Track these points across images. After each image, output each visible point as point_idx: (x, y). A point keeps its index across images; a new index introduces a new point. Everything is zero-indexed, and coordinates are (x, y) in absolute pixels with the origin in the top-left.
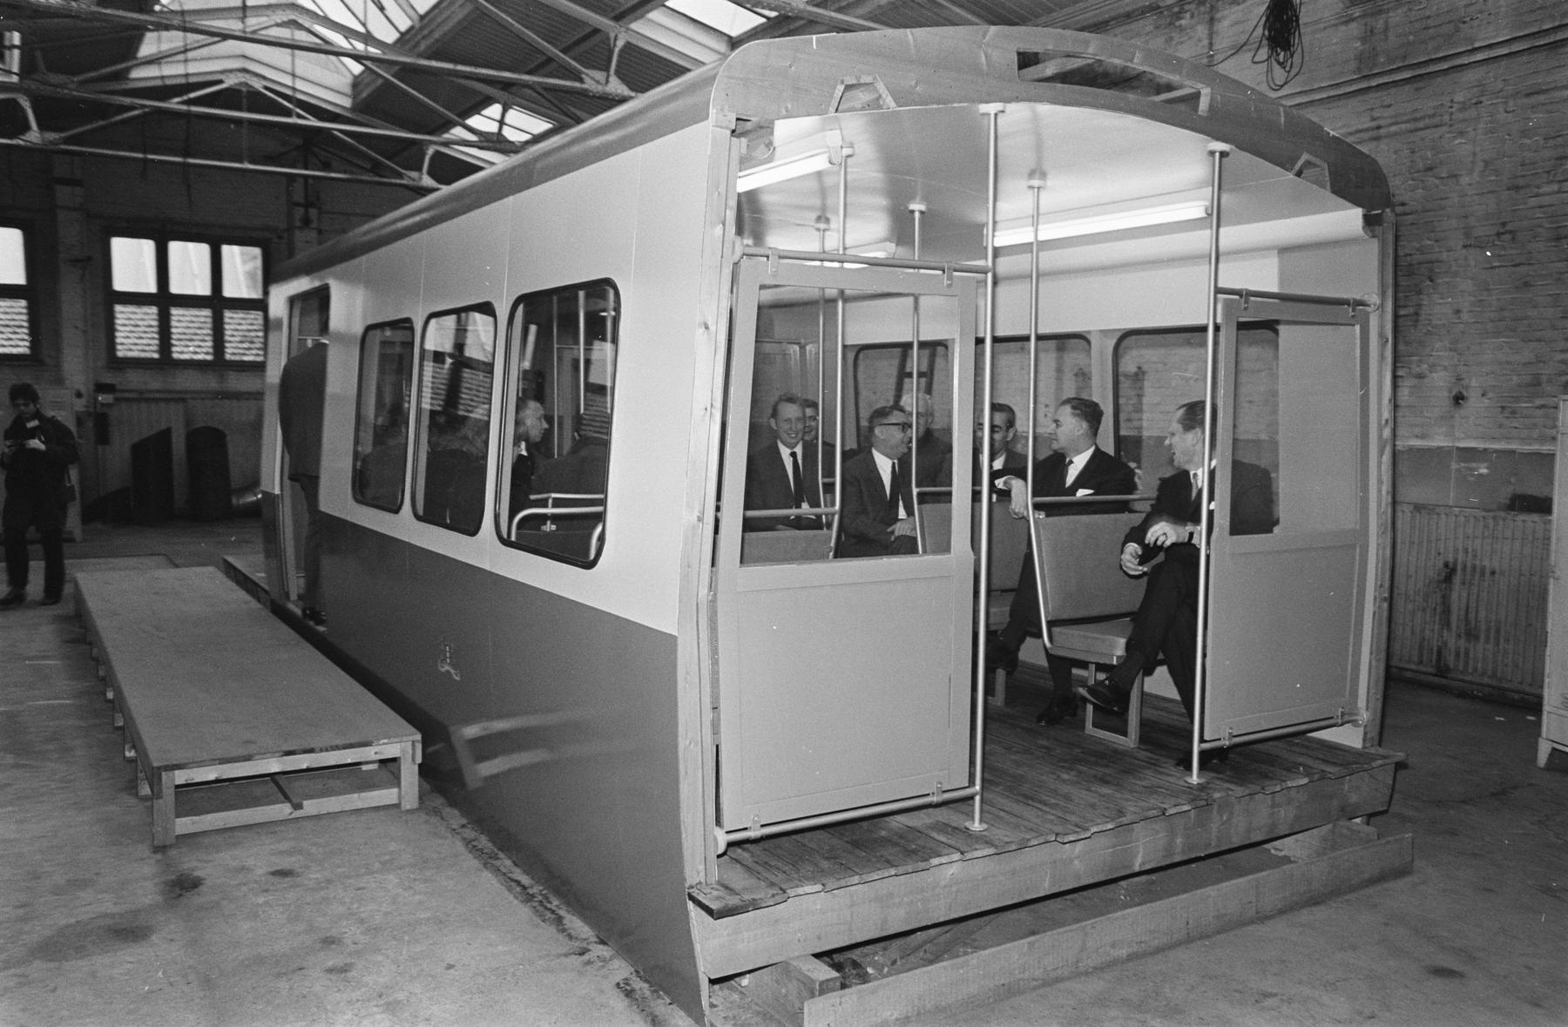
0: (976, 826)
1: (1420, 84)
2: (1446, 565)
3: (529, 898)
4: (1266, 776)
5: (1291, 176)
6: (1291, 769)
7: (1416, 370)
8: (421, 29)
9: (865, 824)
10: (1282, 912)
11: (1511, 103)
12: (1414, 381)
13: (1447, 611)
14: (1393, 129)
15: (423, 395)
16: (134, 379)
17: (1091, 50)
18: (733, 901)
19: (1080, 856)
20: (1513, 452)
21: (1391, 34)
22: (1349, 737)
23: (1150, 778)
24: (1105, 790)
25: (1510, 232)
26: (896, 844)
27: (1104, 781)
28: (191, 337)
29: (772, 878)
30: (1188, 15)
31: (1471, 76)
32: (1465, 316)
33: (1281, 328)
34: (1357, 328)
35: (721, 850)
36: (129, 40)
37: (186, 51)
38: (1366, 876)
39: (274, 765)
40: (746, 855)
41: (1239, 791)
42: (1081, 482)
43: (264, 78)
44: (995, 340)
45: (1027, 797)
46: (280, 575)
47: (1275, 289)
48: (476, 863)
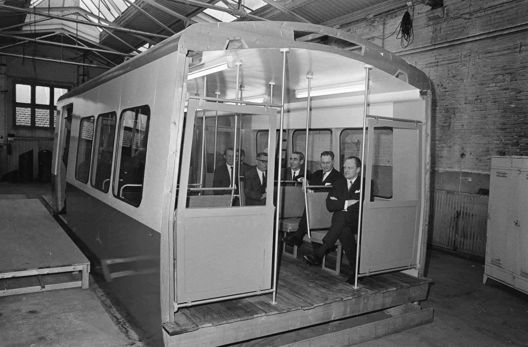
0: (274, 303)
1: (451, 48)
2: (457, 212)
3: (118, 322)
4: (382, 287)
5: (394, 77)
6: (392, 284)
7: (449, 145)
8: (122, 17)
9: (234, 301)
10: (384, 336)
11: (480, 56)
12: (448, 149)
13: (457, 228)
14: (442, 63)
15: (119, 141)
16: (22, 133)
17: (321, 31)
18: (178, 329)
19: (312, 315)
20: (480, 174)
21: (442, 30)
22: (414, 273)
23: (341, 286)
24: (323, 290)
25: (480, 99)
26: (243, 309)
27: (324, 287)
28: (43, 118)
29: (195, 321)
30: (376, 22)
31: (468, 46)
32: (465, 127)
33: (394, 130)
34: (418, 131)
35: (176, 310)
36: (21, 17)
37: (35, 22)
38: (416, 323)
39: (35, 272)
40: (188, 311)
41: (370, 292)
42: (327, 180)
43: (69, 32)
44: (310, 130)
45: (294, 292)
46: (57, 204)
47: (392, 117)
48: (104, 309)
